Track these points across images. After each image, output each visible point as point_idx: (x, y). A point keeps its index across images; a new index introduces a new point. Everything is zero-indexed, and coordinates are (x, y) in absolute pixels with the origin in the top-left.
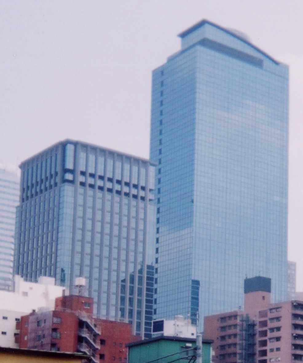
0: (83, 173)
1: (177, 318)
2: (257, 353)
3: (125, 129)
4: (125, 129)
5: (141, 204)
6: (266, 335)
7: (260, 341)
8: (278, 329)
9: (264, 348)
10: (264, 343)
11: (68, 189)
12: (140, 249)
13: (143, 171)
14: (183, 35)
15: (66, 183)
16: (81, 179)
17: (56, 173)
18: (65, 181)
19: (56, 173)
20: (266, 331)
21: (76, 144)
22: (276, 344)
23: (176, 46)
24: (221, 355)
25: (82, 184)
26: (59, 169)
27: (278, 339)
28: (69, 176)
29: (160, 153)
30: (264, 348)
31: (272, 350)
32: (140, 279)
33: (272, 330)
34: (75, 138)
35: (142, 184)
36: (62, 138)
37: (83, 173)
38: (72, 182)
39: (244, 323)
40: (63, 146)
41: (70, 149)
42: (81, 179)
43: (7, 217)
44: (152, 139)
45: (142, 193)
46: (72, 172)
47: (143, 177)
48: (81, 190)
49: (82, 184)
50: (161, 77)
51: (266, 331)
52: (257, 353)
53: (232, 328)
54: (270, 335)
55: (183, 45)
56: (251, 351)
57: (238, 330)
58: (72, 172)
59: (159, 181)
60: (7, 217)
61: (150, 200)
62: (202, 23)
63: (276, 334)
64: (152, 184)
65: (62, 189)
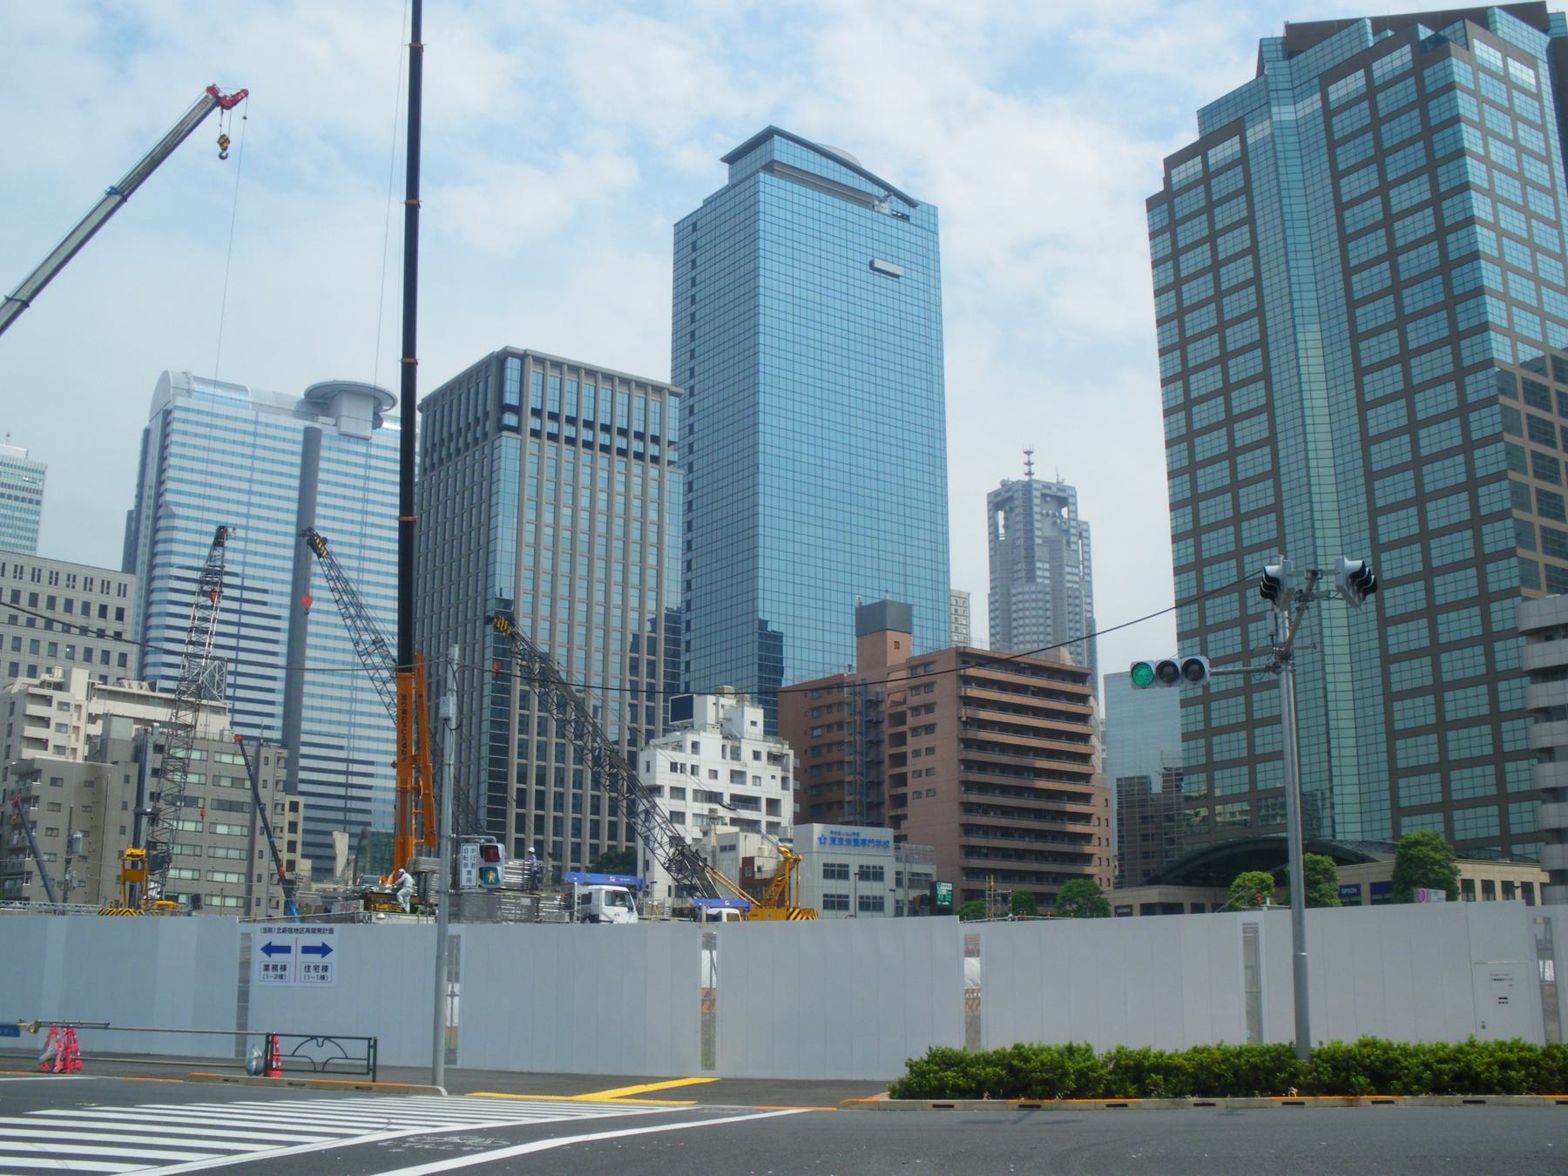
0: (537, 413)
1: (722, 694)
2: (887, 778)
3: (624, 325)
4: (624, 325)
5: (653, 472)
6: (904, 723)
7: (891, 735)
8: (929, 708)
9: (901, 790)
10: (900, 739)
11: (508, 442)
12: (652, 560)
13: (654, 406)
14: (732, 159)
15: (504, 433)
16: (532, 423)
17: (486, 414)
18: (503, 428)
19: (486, 414)
20: (904, 734)
21: (523, 357)
22: (923, 742)
23: (721, 177)
24: (812, 787)
25: (536, 433)
26: (490, 406)
27: (930, 729)
28: (510, 419)
29: (692, 376)
30: (901, 790)
31: (916, 753)
32: (652, 644)
33: (915, 731)
34: (520, 345)
35: (653, 430)
36: (497, 347)
37: (537, 413)
38: (516, 430)
39: (857, 718)
40: (499, 361)
41: (513, 365)
42: (532, 423)
43: (386, 459)
44: (676, 314)
45: (653, 450)
46: (516, 410)
47: (654, 418)
48: (532, 445)
49: (536, 433)
50: (693, 239)
51: (904, 734)
52: (887, 778)
53: (835, 709)
54: (912, 721)
55: (731, 177)
56: (872, 716)
57: (845, 714)
58: (516, 410)
59: (688, 586)
60: (386, 459)
61: (670, 463)
62: (769, 134)
63: (926, 719)
64: (672, 434)
65: (497, 444)
